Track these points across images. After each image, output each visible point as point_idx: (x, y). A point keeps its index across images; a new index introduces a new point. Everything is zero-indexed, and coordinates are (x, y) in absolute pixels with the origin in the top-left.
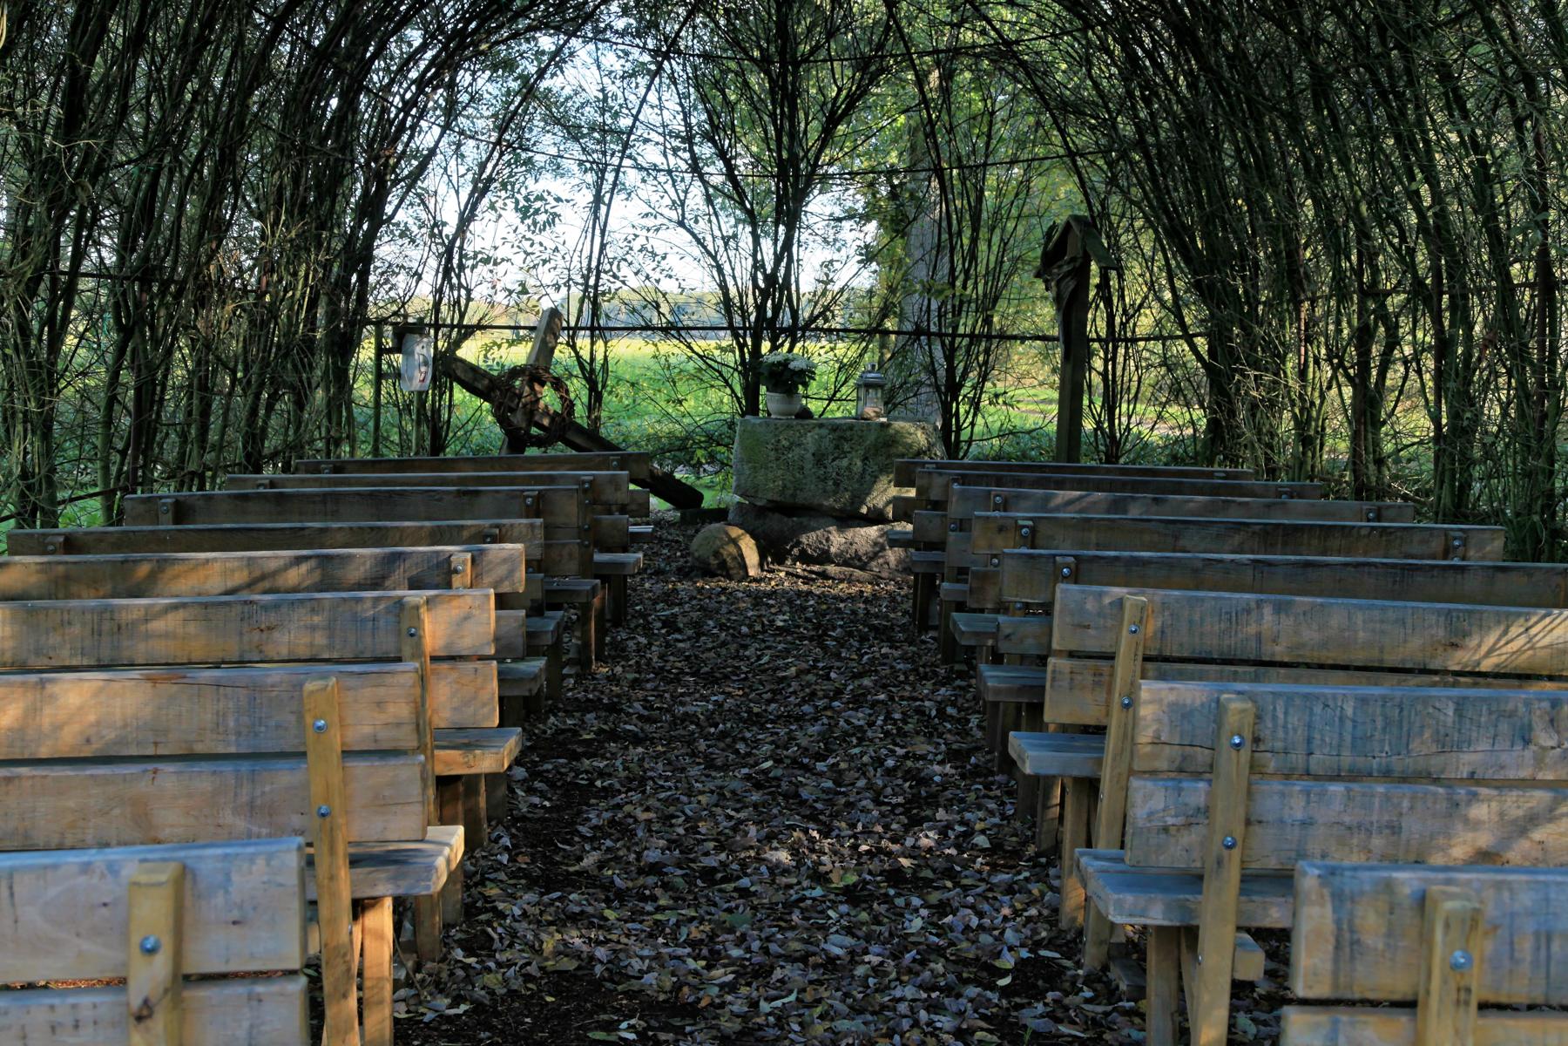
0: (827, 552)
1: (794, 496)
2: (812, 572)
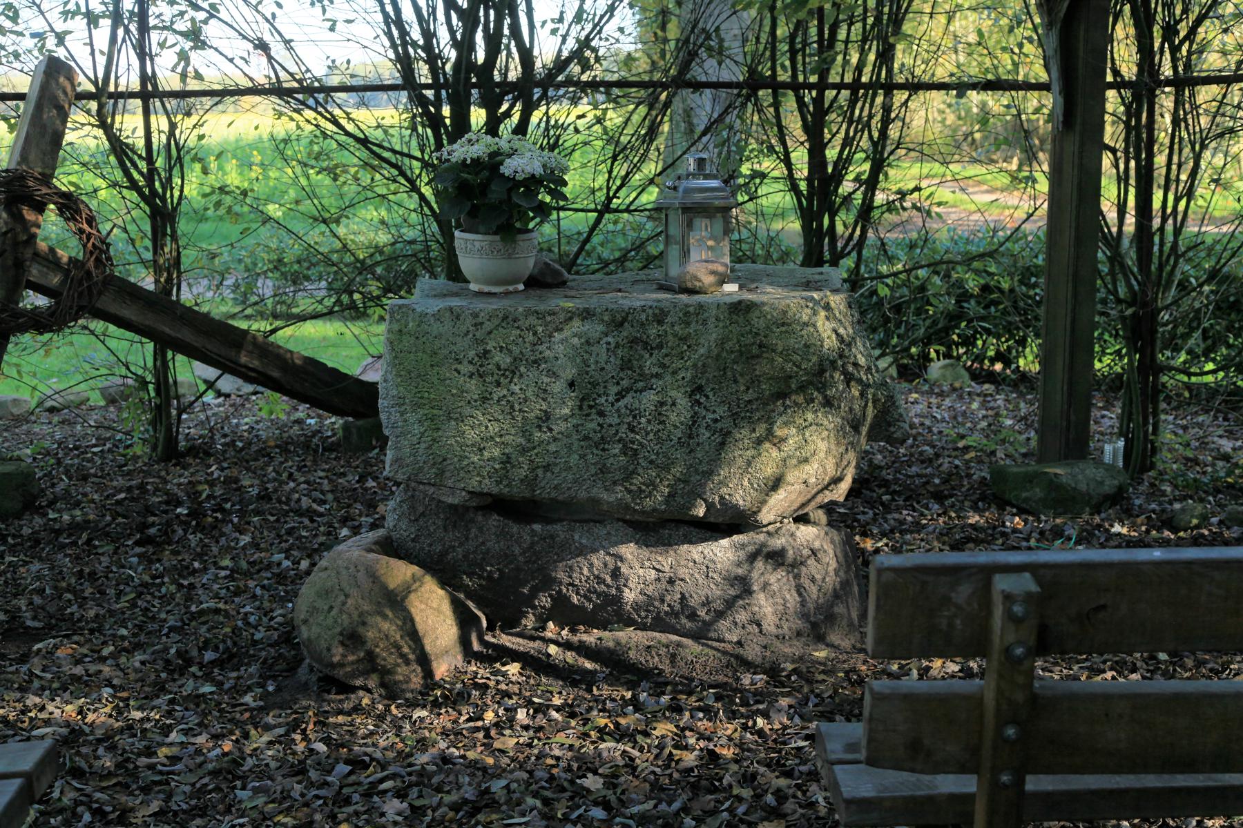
0: (617, 600)
1: (531, 482)
2: (582, 649)
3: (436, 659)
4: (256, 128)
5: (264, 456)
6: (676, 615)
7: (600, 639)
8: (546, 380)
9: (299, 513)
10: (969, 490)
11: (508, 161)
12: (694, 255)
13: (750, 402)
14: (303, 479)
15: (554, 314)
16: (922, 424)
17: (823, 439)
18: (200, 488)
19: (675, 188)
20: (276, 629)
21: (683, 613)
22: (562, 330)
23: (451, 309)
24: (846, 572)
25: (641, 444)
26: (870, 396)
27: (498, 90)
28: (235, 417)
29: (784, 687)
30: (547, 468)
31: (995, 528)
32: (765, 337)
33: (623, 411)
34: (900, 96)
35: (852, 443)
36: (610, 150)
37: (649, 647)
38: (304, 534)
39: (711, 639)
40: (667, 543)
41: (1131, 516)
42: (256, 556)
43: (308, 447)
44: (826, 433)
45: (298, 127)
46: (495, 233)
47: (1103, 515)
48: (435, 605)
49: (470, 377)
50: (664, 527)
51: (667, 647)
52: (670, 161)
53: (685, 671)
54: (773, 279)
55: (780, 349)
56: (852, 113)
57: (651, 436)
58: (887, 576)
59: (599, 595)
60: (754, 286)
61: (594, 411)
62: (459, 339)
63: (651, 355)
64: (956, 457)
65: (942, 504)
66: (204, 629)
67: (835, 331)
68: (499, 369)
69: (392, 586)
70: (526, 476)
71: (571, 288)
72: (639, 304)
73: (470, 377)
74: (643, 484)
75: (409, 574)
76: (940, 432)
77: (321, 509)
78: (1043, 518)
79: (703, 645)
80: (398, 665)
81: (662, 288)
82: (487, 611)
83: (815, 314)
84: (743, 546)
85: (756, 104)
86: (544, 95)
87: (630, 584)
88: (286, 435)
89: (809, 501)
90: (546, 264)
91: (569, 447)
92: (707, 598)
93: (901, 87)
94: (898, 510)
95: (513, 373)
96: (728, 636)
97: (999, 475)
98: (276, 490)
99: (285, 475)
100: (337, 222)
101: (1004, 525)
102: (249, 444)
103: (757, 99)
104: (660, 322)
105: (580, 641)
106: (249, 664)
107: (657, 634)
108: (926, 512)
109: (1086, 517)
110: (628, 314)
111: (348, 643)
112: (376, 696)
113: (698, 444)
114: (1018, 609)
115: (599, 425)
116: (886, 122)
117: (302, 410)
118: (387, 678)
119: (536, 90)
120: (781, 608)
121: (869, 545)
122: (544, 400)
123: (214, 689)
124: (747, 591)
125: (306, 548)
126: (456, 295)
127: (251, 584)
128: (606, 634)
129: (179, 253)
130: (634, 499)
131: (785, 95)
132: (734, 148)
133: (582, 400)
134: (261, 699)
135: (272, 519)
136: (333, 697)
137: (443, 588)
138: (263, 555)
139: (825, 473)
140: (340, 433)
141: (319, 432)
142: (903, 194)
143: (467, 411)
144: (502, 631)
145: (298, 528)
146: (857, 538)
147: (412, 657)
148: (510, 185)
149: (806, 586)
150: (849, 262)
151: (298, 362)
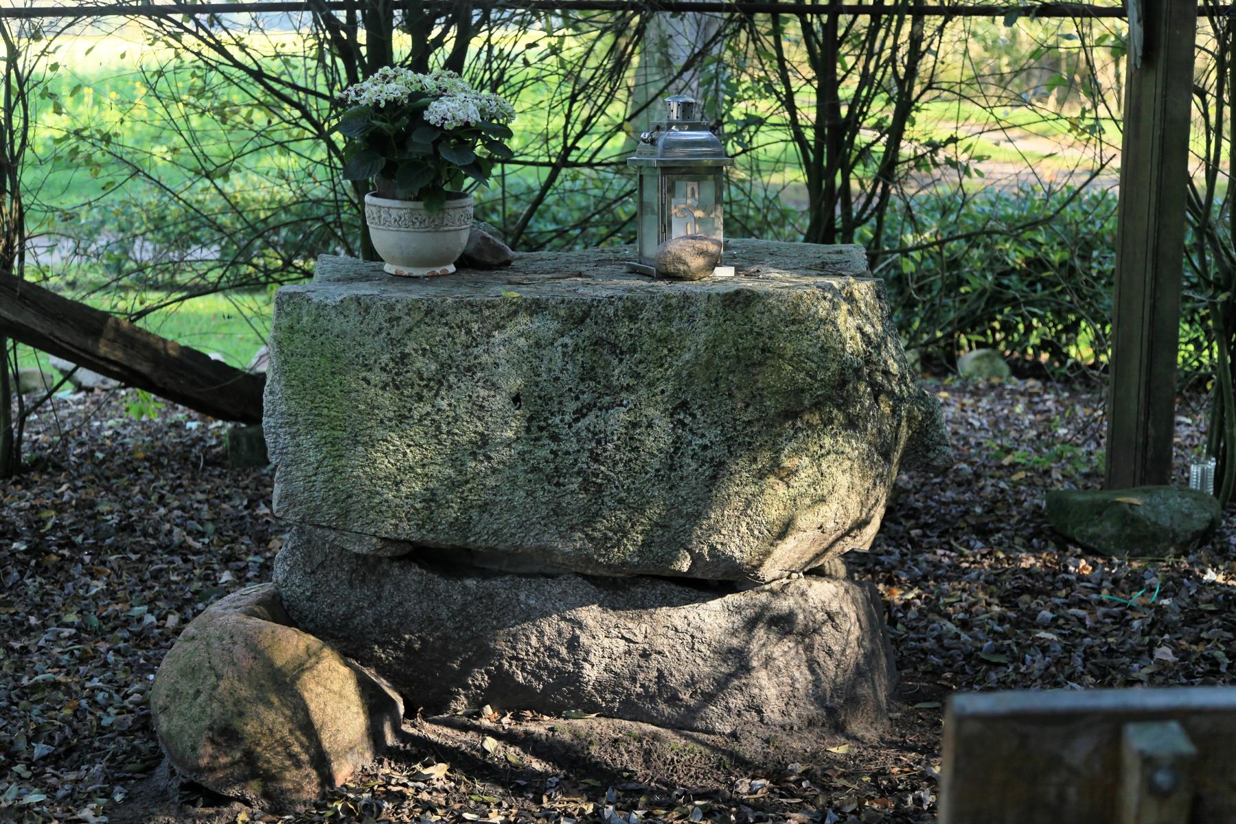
0: (575, 679)
1: (462, 526)
2: (528, 743)
3: (337, 759)
4: (123, 56)
5: (129, 472)
6: (652, 698)
7: (552, 729)
8: (484, 393)
9: (170, 549)
10: (1019, 522)
11: (434, 104)
12: (677, 230)
13: (749, 423)
14: (176, 504)
15: (494, 307)
16: (955, 433)
17: (844, 472)
18: (45, 514)
19: (653, 142)
20: (130, 712)
21: (660, 695)
22: (504, 327)
23: (358, 300)
24: (872, 641)
25: (606, 477)
26: (903, 413)
27: (426, 11)
28: (96, 419)
29: (793, 797)
30: (484, 508)
31: (1055, 574)
32: (770, 338)
33: (584, 434)
34: (932, 22)
35: (880, 476)
36: (568, 90)
37: (616, 741)
38: (174, 578)
39: (696, 730)
40: (641, 605)
41: (1226, 558)
42: (110, 609)
43: (186, 459)
44: (848, 463)
45: (178, 56)
46: (417, 199)
47: (1191, 557)
48: (336, 687)
49: (383, 388)
50: (635, 584)
51: (640, 741)
52: (642, 101)
53: (663, 774)
54: (778, 259)
55: (789, 353)
56: (872, 45)
57: (620, 467)
58: (972, 728)
59: (551, 672)
60: (753, 269)
61: (545, 433)
62: (368, 339)
63: (621, 360)
64: (1000, 478)
65: (986, 542)
66: (36, 710)
67: (860, 329)
68: (422, 379)
69: (279, 662)
70: (457, 519)
71: (516, 270)
72: (604, 294)
73: (383, 388)
74: (610, 529)
75: (302, 646)
76: (979, 444)
77: (198, 545)
78: (1116, 560)
79: (687, 737)
80: (285, 768)
81: (635, 272)
82: (405, 690)
83: (834, 308)
84: (738, 609)
85: (751, 32)
86: (485, 18)
87: (592, 658)
88: (158, 443)
89: (826, 550)
90: (484, 238)
91: (513, 481)
92: (692, 677)
93: (933, 11)
94: (931, 548)
95: (440, 383)
96: (719, 726)
97: (1059, 504)
98: (141, 519)
99: (154, 498)
100: (225, 176)
101: (1066, 571)
102: (112, 454)
103: (752, 25)
104: (633, 319)
105: (526, 732)
106: (92, 762)
107: (627, 723)
108: (967, 552)
109: (1170, 560)
110: (590, 307)
111: (220, 740)
112: (256, 809)
113: (682, 478)
114: (1162, 778)
115: (552, 452)
116: (916, 54)
117: (181, 413)
118: (272, 786)
119: (475, 12)
120: (787, 689)
121: (897, 596)
122: (479, 419)
123: (43, 797)
124: (744, 668)
125: (175, 598)
126: (366, 278)
127: (103, 647)
128: (560, 723)
129: (22, 215)
130: (597, 549)
131: (787, 20)
132: (723, 86)
133: (530, 419)
134: (104, 814)
135: (134, 557)
136: (199, 810)
137: (347, 665)
138: (118, 607)
139: (847, 515)
140: (227, 443)
141: (201, 439)
142: (934, 147)
143: (379, 433)
144: (425, 718)
145: (167, 571)
146: (881, 587)
147: (304, 757)
148: (438, 135)
149: (821, 660)
150: (867, 231)
151: (172, 352)
